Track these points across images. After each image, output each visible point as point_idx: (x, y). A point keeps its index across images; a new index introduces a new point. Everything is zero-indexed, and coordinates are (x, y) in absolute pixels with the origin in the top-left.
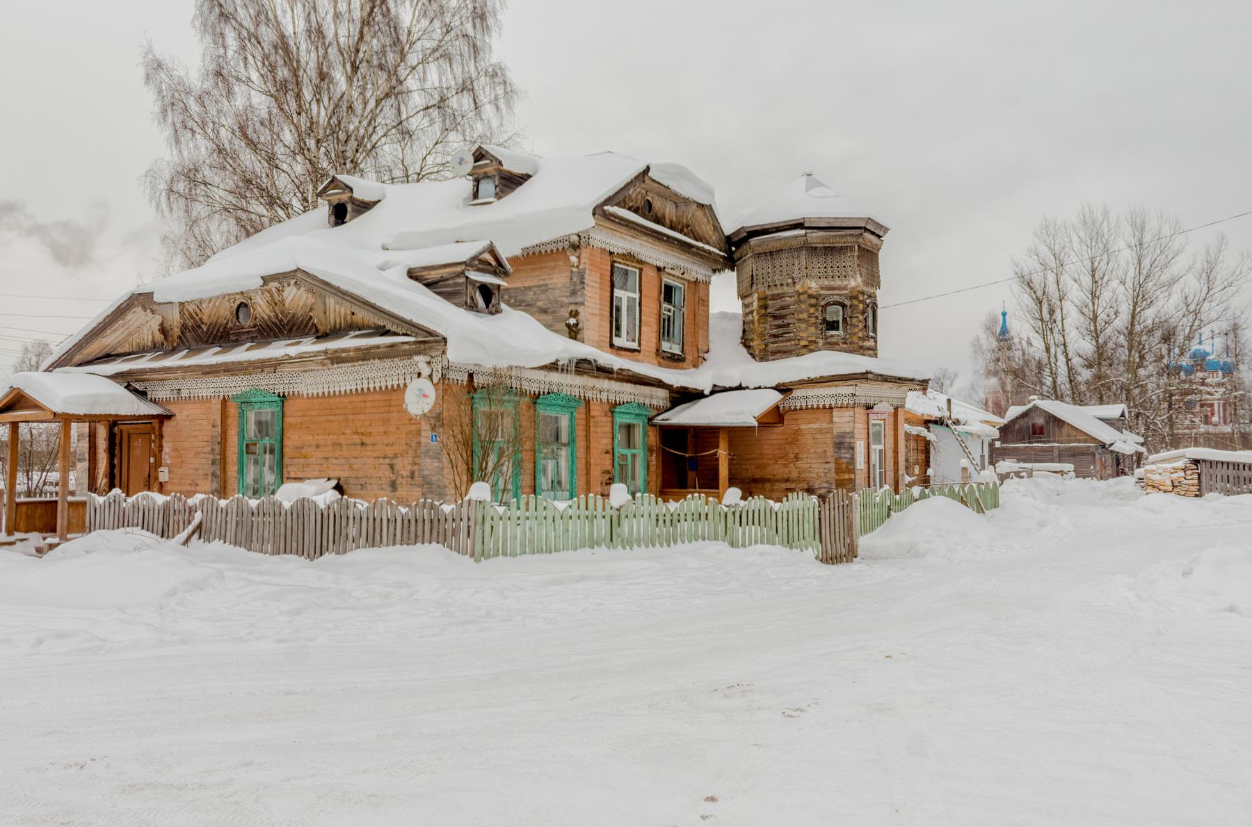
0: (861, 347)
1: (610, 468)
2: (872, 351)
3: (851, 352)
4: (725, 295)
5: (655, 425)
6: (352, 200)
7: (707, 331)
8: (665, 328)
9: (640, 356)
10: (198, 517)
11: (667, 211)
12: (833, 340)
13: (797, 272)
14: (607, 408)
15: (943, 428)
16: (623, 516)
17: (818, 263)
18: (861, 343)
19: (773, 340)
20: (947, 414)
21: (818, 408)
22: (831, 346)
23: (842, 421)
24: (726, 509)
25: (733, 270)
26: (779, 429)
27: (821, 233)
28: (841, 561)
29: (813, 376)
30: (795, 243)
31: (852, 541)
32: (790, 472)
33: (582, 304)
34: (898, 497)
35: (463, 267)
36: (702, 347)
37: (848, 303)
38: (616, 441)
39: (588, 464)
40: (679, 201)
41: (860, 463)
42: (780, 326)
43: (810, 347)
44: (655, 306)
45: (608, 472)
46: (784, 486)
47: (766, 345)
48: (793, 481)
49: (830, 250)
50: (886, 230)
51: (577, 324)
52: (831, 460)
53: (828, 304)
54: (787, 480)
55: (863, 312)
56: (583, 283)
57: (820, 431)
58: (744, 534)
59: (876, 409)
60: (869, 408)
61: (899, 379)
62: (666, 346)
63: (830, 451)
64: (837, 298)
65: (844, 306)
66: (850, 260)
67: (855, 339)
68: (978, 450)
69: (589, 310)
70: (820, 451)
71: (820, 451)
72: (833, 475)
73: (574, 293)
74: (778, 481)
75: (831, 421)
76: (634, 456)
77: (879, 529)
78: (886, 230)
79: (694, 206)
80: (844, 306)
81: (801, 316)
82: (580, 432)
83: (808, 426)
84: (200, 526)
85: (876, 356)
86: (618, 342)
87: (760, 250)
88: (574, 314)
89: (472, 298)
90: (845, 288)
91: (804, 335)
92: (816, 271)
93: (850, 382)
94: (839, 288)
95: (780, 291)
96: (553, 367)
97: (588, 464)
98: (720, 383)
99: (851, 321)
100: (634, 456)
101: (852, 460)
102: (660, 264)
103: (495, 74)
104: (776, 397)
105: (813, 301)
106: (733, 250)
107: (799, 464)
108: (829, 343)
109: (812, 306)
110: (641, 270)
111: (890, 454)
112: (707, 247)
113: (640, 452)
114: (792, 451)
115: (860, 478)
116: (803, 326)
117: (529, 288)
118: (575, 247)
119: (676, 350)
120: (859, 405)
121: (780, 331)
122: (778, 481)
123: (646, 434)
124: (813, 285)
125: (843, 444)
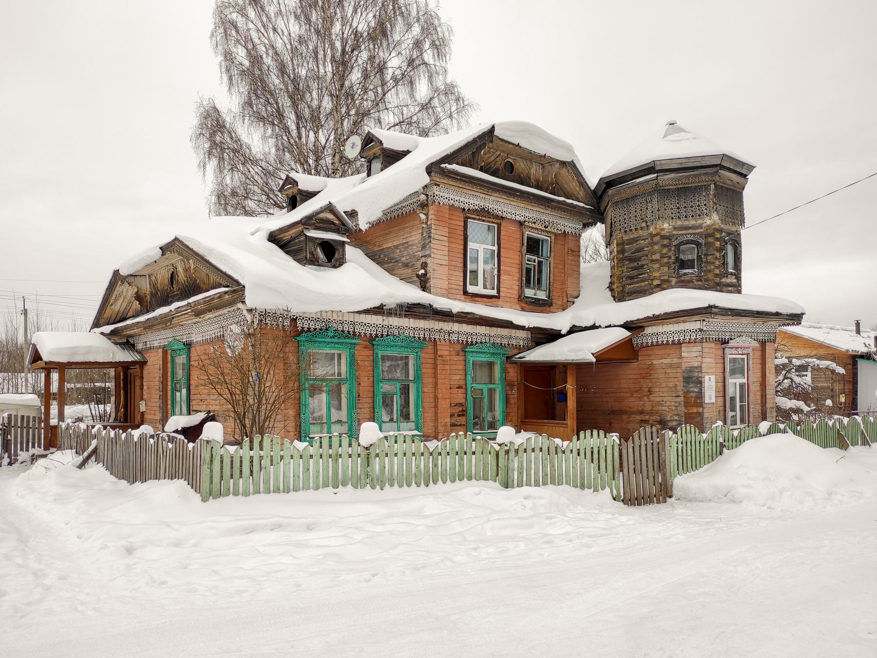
0: (718, 284)
1: (463, 401)
2: (736, 288)
3: (706, 289)
5: (515, 363)
6: (300, 191)
7: (578, 279)
8: (529, 277)
9: (500, 302)
10: (94, 443)
11: (533, 171)
13: (649, 215)
14: (459, 347)
15: (870, 362)
16: (373, 455)
17: (672, 204)
18: (717, 280)
19: (629, 282)
21: (668, 344)
22: (685, 284)
23: (690, 355)
24: (497, 448)
26: (635, 365)
27: (672, 175)
28: (651, 502)
29: (657, 313)
30: (648, 187)
31: (665, 480)
32: (644, 405)
33: (429, 256)
35: (300, 228)
36: (571, 291)
38: (469, 378)
39: (436, 398)
40: (544, 161)
42: (635, 269)
43: (664, 285)
44: (516, 258)
45: (461, 405)
46: (638, 418)
47: (624, 287)
48: (648, 413)
49: (683, 192)
50: (751, 168)
51: (425, 274)
52: (681, 393)
55: (720, 250)
56: (430, 237)
57: (671, 366)
58: (581, 464)
59: (732, 343)
60: (725, 342)
61: (758, 313)
62: (529, 293)
63: (680, 385)
64: (689, 237)
65: (698, 245)
66: (708, 198)
67: (710, 276)
69: (436, 261)
71: (671, 385)
72: (683, 409)
73: (424, 247)
74: (633, 413)
75: (681, 357)
76: (491, 392)
78: (751, 168)
79: (557, 165)
80: (698, 245)
81: (654, 257)
82: (427, 370)
83: (661, 361)
84: (95, 451)
85: (739, 292)
86: (471, 289)
87: (616, 199)
88: (424, 266)
89: (312, 254)
90: (700, 227)
91: (657, 274)
92: (669, 212)
93: (696, 318)
94: (694, 227)
96: (379, 310)
97: (436, 398)
99: (714, 259)
100: (491, 392)
101: (700, 395)
102: (522, 219)
103: (450, 90)
104: (624, 334)
105: (666, 242)
106: (601, 201)
108: (683, 281)
109: (664, 246)
110: (499, 225)
111: (755, 388)
112: (575, 203)
113: (499, 388)
114: (645, 385)
116: (656, 266)
117: (396, 247)
118: (424, 206)
119: (542, 295)
121: (635, 272)
122: (633, 413)
123: (504, 371)
125: (693, 379)
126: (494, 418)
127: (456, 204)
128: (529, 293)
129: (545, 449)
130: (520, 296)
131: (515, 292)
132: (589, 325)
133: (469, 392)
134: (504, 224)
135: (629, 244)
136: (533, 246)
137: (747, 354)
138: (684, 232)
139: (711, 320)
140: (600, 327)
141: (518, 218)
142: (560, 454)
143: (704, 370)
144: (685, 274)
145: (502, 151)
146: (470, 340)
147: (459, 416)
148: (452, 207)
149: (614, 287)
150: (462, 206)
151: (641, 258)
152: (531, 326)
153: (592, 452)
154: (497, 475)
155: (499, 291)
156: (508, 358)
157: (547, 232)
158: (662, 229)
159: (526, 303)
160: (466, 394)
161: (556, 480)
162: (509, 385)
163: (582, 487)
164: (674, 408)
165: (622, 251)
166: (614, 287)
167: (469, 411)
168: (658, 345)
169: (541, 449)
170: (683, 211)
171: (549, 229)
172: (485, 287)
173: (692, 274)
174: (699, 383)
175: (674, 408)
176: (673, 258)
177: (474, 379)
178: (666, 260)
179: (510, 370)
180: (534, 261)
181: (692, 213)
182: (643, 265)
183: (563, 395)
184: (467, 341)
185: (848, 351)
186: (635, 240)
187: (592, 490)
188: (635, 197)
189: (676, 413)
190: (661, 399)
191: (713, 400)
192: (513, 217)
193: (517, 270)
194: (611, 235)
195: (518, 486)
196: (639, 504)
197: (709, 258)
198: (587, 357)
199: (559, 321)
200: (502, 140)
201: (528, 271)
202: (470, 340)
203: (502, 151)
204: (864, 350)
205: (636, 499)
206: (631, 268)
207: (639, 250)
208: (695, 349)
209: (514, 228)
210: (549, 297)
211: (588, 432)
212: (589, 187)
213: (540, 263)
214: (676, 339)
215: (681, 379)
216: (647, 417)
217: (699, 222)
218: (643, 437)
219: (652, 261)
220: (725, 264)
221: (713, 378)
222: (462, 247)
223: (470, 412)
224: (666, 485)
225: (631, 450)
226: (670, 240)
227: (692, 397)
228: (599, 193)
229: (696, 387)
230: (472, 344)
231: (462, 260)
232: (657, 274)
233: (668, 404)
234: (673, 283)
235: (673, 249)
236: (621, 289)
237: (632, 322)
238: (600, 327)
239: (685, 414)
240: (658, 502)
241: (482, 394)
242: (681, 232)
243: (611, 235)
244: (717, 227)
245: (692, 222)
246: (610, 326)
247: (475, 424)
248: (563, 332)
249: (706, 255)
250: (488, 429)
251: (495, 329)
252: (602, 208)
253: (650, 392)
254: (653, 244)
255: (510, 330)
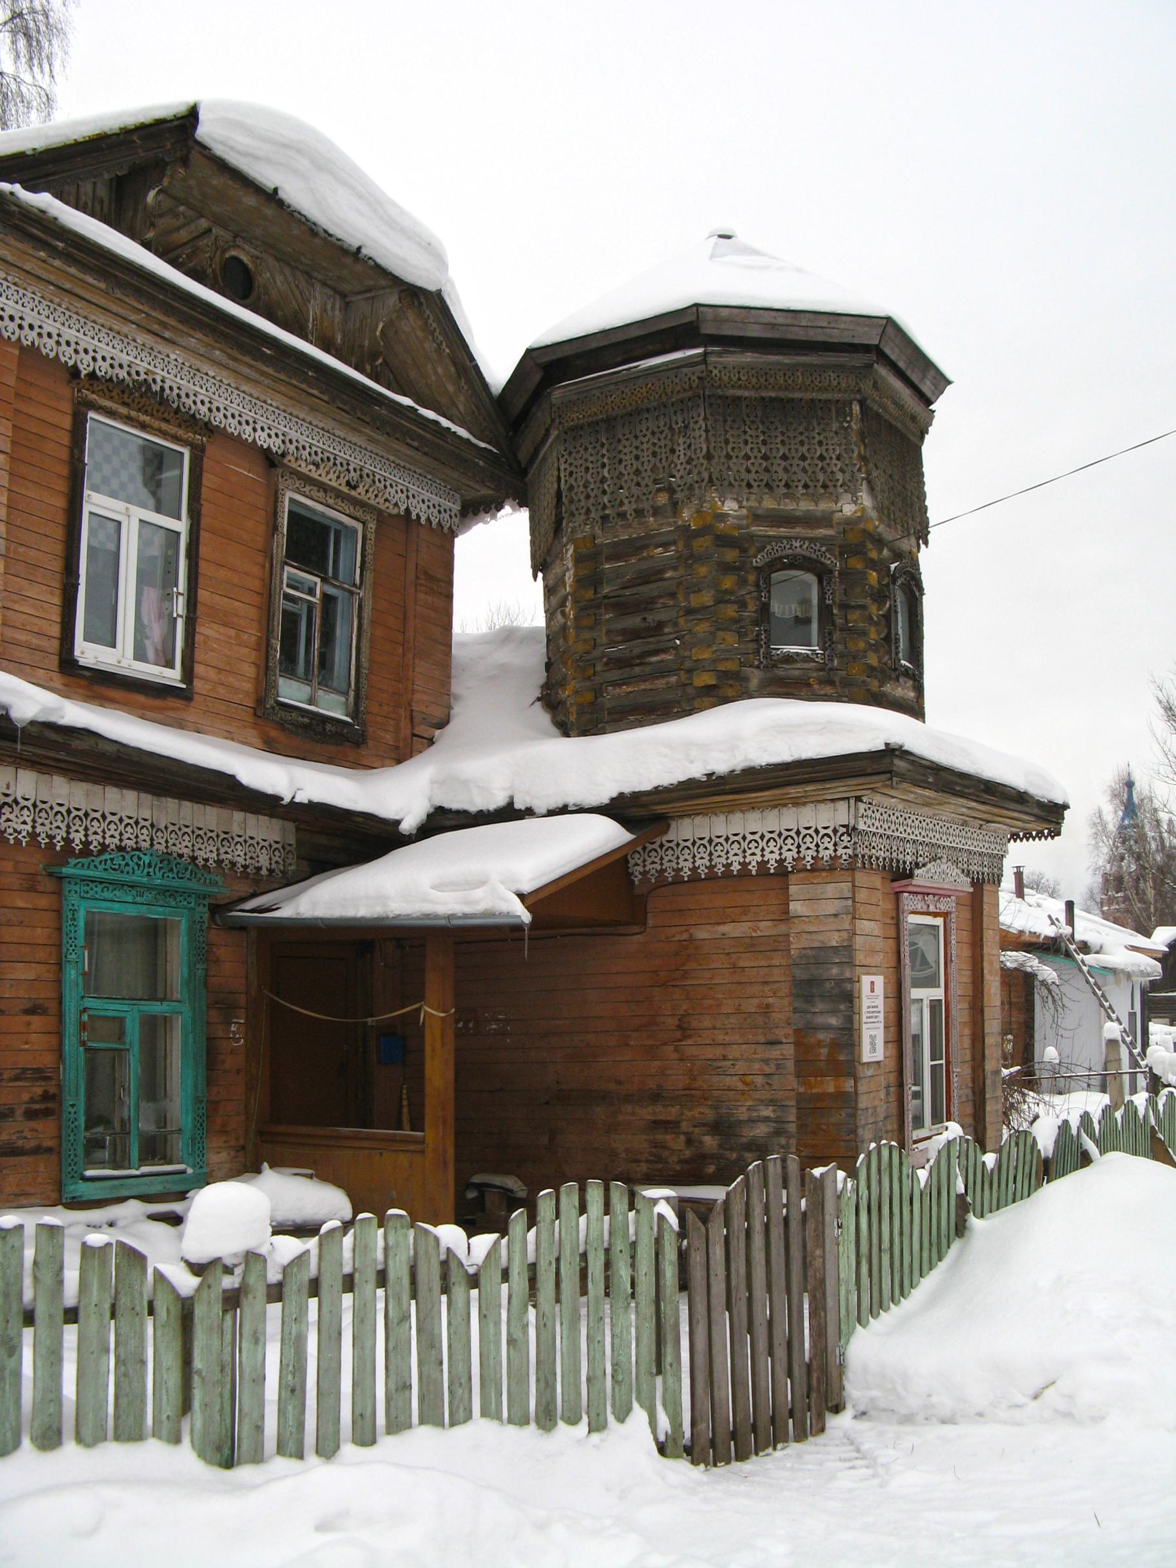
1: (48, 1060)
4: (496, 576)
5: (241, 927)
8: (292, 641)
12: (794, 671)
14: (36, 863)
19: (615, 675)
20: (1067, 930)
23: (814, 908)
25: (521, 505)
27: (748, 358)
34: (990, 1159)
36: (422, 702)
37: (833, 562)
38: (71, 974)
41: (873, 1044)
42: (632, 635)
43: (723, 690)
45: (40, 1075)
46: (647, 1113)
47: (598, 692)
49: (779, 410)
53: (776, 565)
54: (656, 1097)
57: (751, 945)
59: (921, 877)
60: (900, 874)
63: (782, 1006)
65: (823, 574)
68: (1124, 1002)
70: (751, 1006)
71: (751, 1006)
72: (792, 1082)
74: (628, 1099)
75: (785, 916)
76: (154, 1028)
77: (928, 1284)
81: (695, 601)
86: (88, 653)
87: (574, 417)
90: (825, 520)
93: (839, 788)
94: (809, 520)
95: (635, 532)
98: (455, 802)
100: (154, 1028)
101: (849, 1036)
102: (275, 444)
105: (731, 555)
107: (690, 1048)
109: (726, 568)
111: (960, 1013)
115: (872, 1098)
116: (702, 628)
119: (333, 707)
120: (868, 864)
121: (637, 646)
123: (203, 954)
124: (730, 506)
125: (823, 987)
126: (162, 1120)
127: (48, 347)
128: (292, 692)
129: (398, 1271)
130: (260, 702)
131: (244, 681)
132: (492, 807)
133: (71, 1028)
134: (213, 451)
135: (610, 558)
136: (310, 542)
137: (945, 915)
138: (783, 531)
139: (877, 798)
140: (529, 812)
141: (262, 439)
142: (458, 1291)
143: (860, 958)
144: (789, 659)
145: (217, 220)
146: (78, 837)
147: (31, 1115)
148: (30, 353)
149: (565, 694)
150: (67, 356)
151: (652, 601)
152: (302, 798)
153: (584, 1274)
154: (186, 1406)
155: (188, 674)
156: (217, 909)
157: (357, 503)
158: (722, 517)
159: (281, 725)
160: (60, 1034)
161: (443, 1408)
162: (218, 1004)
163: (547, 1419)
164: (759, 1080)
165: (590, 580)
166: (565, 694)
167: (69, 1100)
168: (712, 876)
169: (382, 1279)
170: (778, 466)
171: (360, 493)
172: (140, 655)
173: (807, 659)
174: (848, 998)
175: (759, 1080)
176: (752, 606)
177: (92, 983)
178: (731, 611)
179: (222, 952)
180: (311, 592)
181: (804, 478)
182: (660, 625)
183: (404, 1043)
184: (68, 841)
185: (1021, 932)
186: (635, 547)
187: (583, 1426)
188: (635, 414)
189: (764, 1095)
190: (719, 1051)
191: (879, 1055)
192: (247, 433)
193: (252, 612)
194: (558, 529)
195: (292, 1447)
196: (742, 1457)
197: (854, 616)
198: (503, 907)
199: (396, 793)
200: (222, 166)
201: (291, 620)
202: (78, 837)
203: (217, 220)
204: (1049, 931)
205: (734, 1435)
206: (624, 632)
207: (647, 578)
208: (831, 889)
209: (247, 471)
210: (355, 713)
211: (569, 1194)
212: (485, 385)
213: (328, 599)
214: (772, 859)
215: (785, 989)
216: (673, 1112)
217: (824, 506)
218: (764, 1192)
219: (690, 611)
220: (889, 640)
221: (879, 981)
222: (60, 502)
223: (76, 1103)
224: (824, 1370)
225: (718, 1252)
226: (743, 550)
227: (820, 1044)
228: (519, 403)
229: (833, 1012)
230: (86, 852)
231: (59, 548)
232: (706, 655)
233: (741, 1067)
234: (754, 683)
235: (752, 578)
236: (589, 696)
237: (636, 796)
238: (529, 812)
239: (800, 1098)
240: (801, 1437)
241: (121, 1035)
242: (772, 532)
243: (558, 529)
244: (870, 527)
245: (805, 506)
246: (563, 810)
247: (94, 1145)
248: (408, 825)
249: (844, 607)
250: (143, 1161)
251: (171, 803)
252: (523, 456)
253: (684, 1029)
254: (689, 559)
255: (225, 813)
